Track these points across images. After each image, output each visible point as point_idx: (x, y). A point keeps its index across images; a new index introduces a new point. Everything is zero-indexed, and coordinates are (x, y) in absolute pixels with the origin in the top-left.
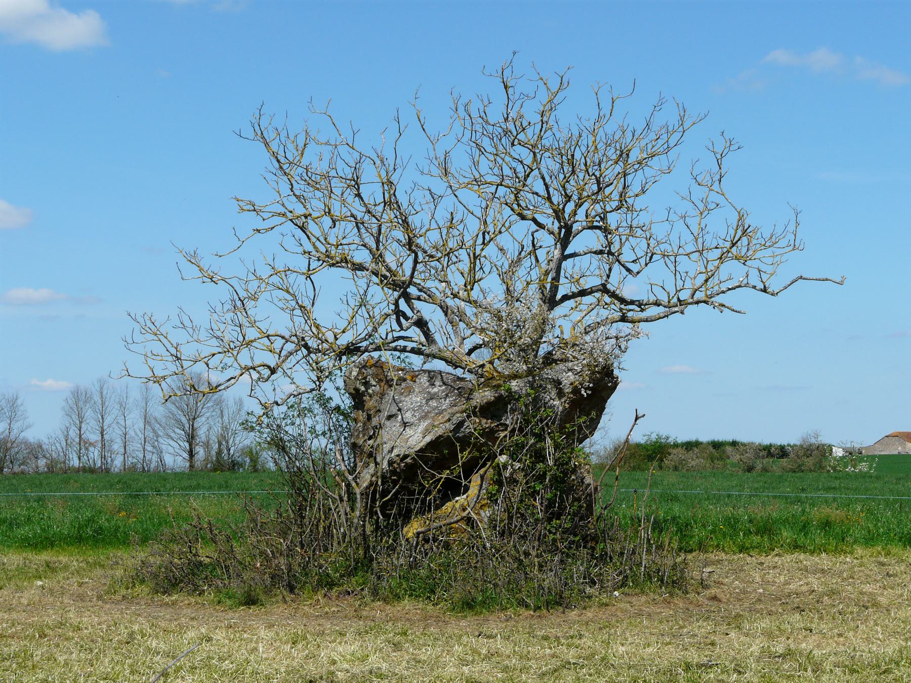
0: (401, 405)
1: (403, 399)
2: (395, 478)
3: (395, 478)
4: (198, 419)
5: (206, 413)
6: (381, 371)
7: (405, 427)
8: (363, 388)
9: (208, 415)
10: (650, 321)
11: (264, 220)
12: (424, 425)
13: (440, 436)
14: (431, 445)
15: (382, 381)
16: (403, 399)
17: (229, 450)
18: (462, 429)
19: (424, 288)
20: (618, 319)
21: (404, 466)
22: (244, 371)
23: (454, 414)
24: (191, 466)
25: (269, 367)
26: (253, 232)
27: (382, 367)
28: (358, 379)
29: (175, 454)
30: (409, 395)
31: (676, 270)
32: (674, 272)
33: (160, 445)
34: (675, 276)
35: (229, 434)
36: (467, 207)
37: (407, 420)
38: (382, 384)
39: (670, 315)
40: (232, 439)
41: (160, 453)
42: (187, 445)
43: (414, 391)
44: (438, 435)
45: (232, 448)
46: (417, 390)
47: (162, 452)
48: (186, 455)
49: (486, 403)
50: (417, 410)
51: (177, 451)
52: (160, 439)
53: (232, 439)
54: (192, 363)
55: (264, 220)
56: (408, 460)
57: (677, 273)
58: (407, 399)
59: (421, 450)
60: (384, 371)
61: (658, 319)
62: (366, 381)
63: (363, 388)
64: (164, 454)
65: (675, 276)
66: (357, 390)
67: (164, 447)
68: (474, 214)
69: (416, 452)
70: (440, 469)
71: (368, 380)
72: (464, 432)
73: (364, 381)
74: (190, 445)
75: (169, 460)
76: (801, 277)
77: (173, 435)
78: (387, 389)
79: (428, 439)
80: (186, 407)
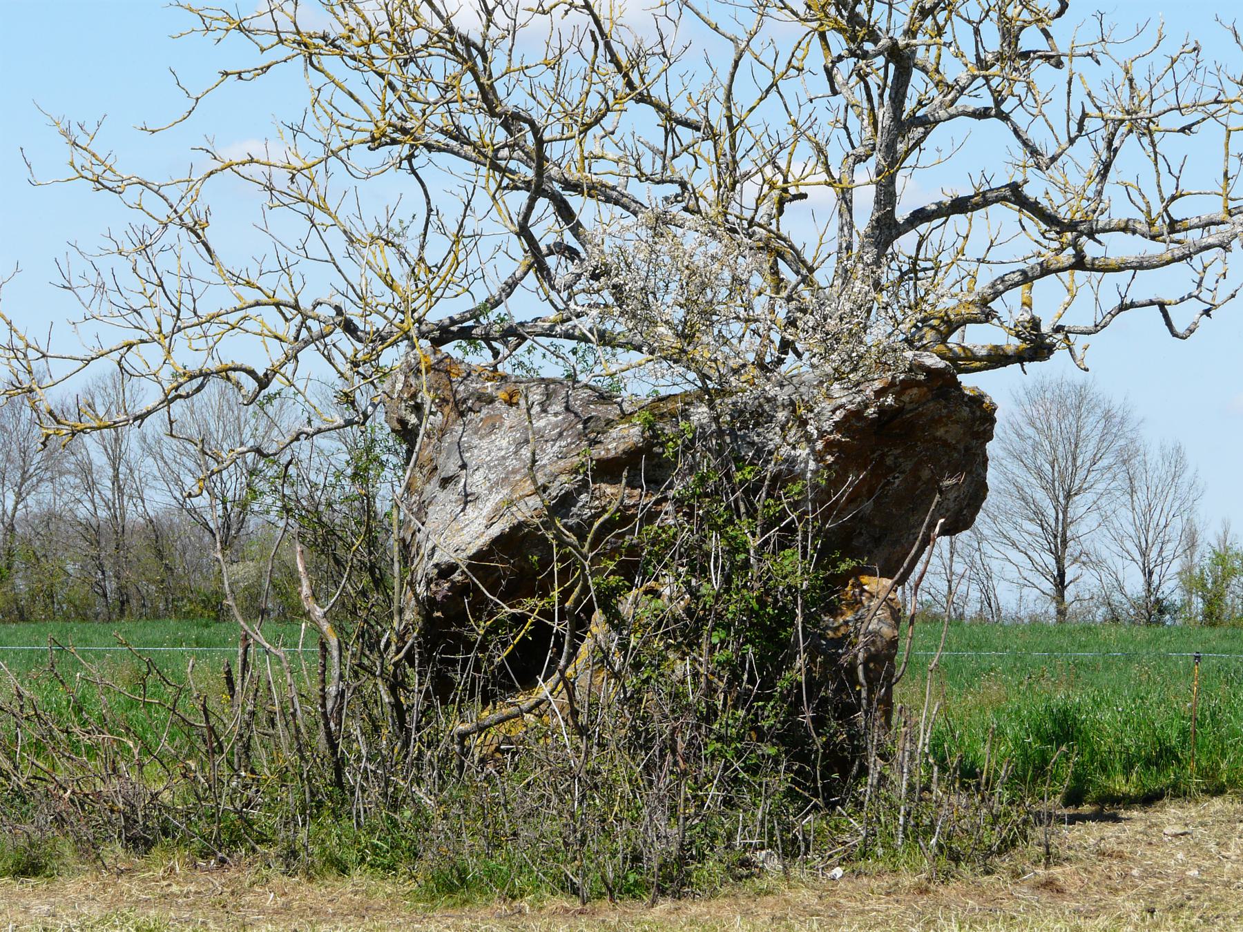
0: (468, 455)
1: (475, 442)
2: (439, 614)
3: (439, 614)
4: (1076, 498)
5: (1096, 482)
6: (445, 381)
7: (466, 503)
8: (413, 419)
9: (1100, 487)
10: (1147, 268)
11: (262, 50)
12: (496, 498)
13: (521, 525)
14: (498, 541)
15: (447, 402)
16: (475, 442)
17: (1151, 573)
18: (574, 510)
19: (623, 195)
20: (1066, 264)
21: (450, 589)
22: (181, 380)
23: (556, 477)
24: (1061, 613)
25: (251, 373)
26: (219, 76)
27: (448, 372)
28: (402, 399)
29: (1022, 581)
30: (490, 433)
31: (1156, 153)
32: (1153, 157)
33: (987, 560)
34: (1156, 165)
35: (1151, 534)
36: (704, 14)
37: (474, 489)
38: (447, 410)
39: (1196, 252)
40: (1156, 549)
41: (985, 579)
42: (1050, 560)
43: (502, 424)
44: (515, 522)
45: (1157, 570)
46: (507, 423)
47: (989, 577)
48: (1048, 586)
49: (624, 452)
50: (495, 466)
51: (1025, 574)
52: (985, 546)
53: (1156, 549)
54: (81, 364)
55: (262, 50)
56: (457, 577)
57: (1160, 158)
58: (484, 443)
59: (480, 555)
60: (451, 382)
61: (1168, 263)
62: (416, 403)
63: (413, 419)
64: (995, 583)
65: (1156, 165)
66: (402, 422)
67: (995, 565)
68: (721, 30)
69: (470, 558)
70: (510, 595)
71: (419, 401)
72: (578, 516)
73: (412, 403)
74: (1059, 560)
75: (1008, 599)
76: (1170, 172)
77: (1014, 535)
78: (454, 421)
79: (495, 531)
80: (1048, 466)
